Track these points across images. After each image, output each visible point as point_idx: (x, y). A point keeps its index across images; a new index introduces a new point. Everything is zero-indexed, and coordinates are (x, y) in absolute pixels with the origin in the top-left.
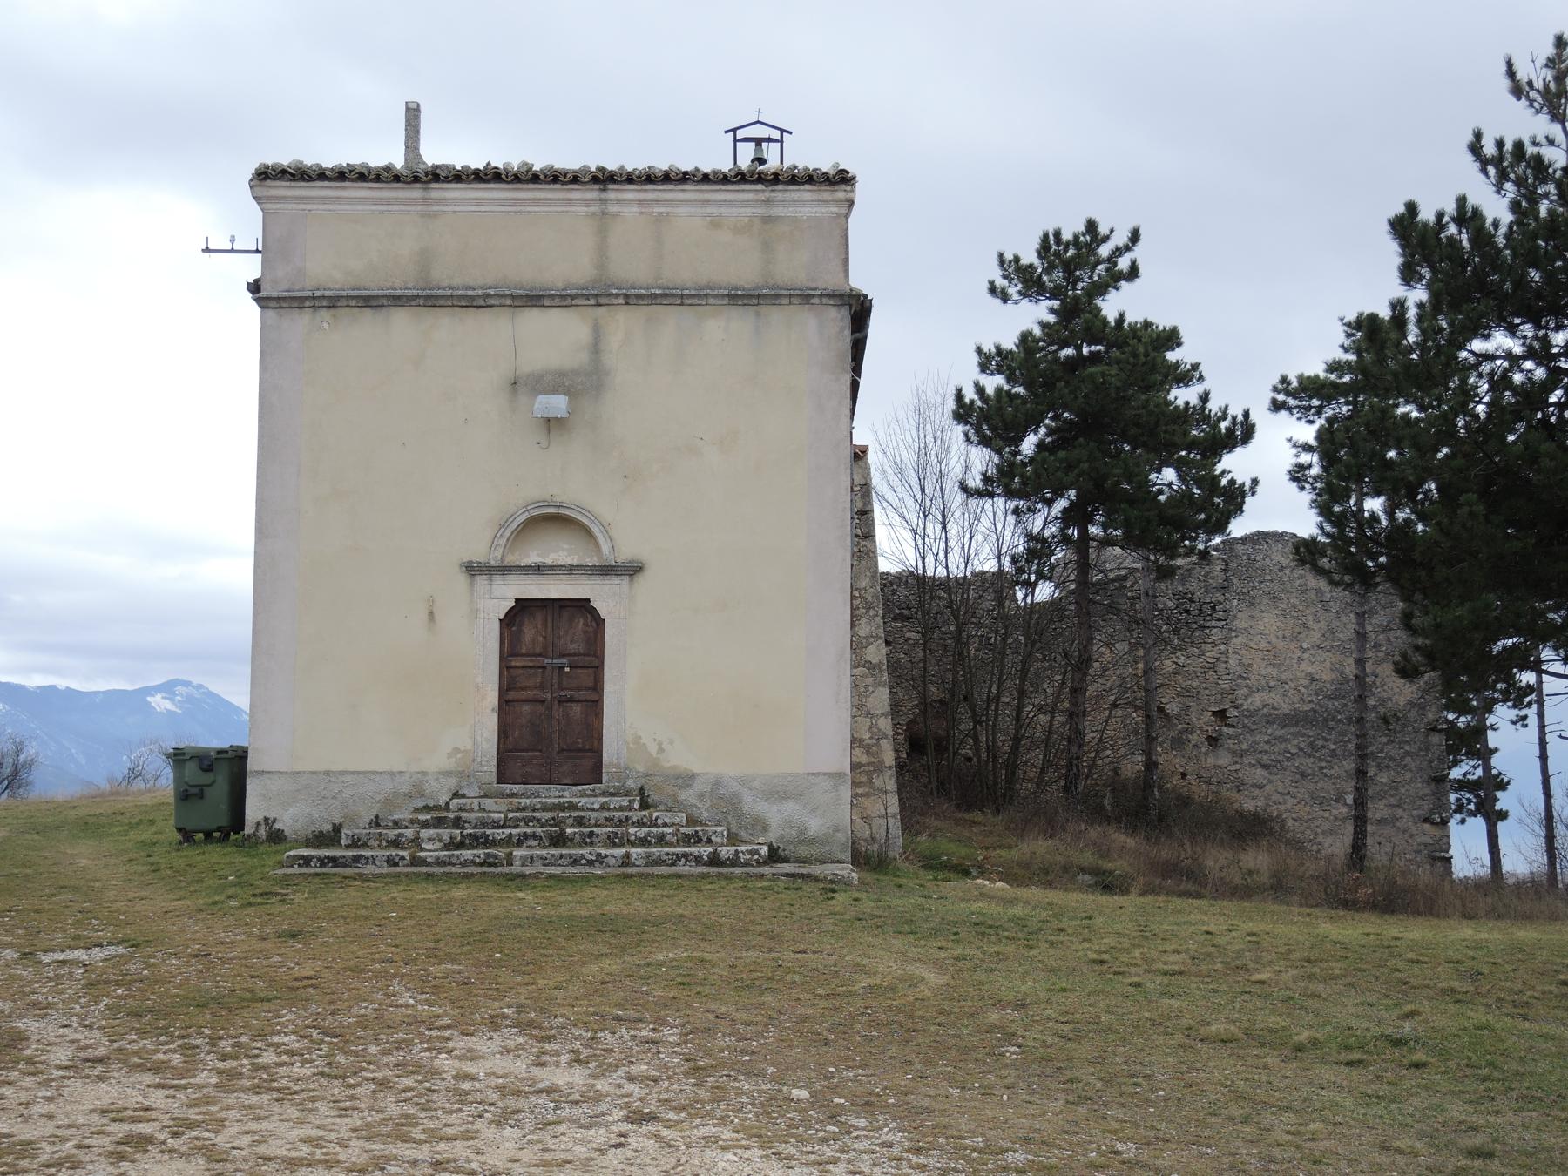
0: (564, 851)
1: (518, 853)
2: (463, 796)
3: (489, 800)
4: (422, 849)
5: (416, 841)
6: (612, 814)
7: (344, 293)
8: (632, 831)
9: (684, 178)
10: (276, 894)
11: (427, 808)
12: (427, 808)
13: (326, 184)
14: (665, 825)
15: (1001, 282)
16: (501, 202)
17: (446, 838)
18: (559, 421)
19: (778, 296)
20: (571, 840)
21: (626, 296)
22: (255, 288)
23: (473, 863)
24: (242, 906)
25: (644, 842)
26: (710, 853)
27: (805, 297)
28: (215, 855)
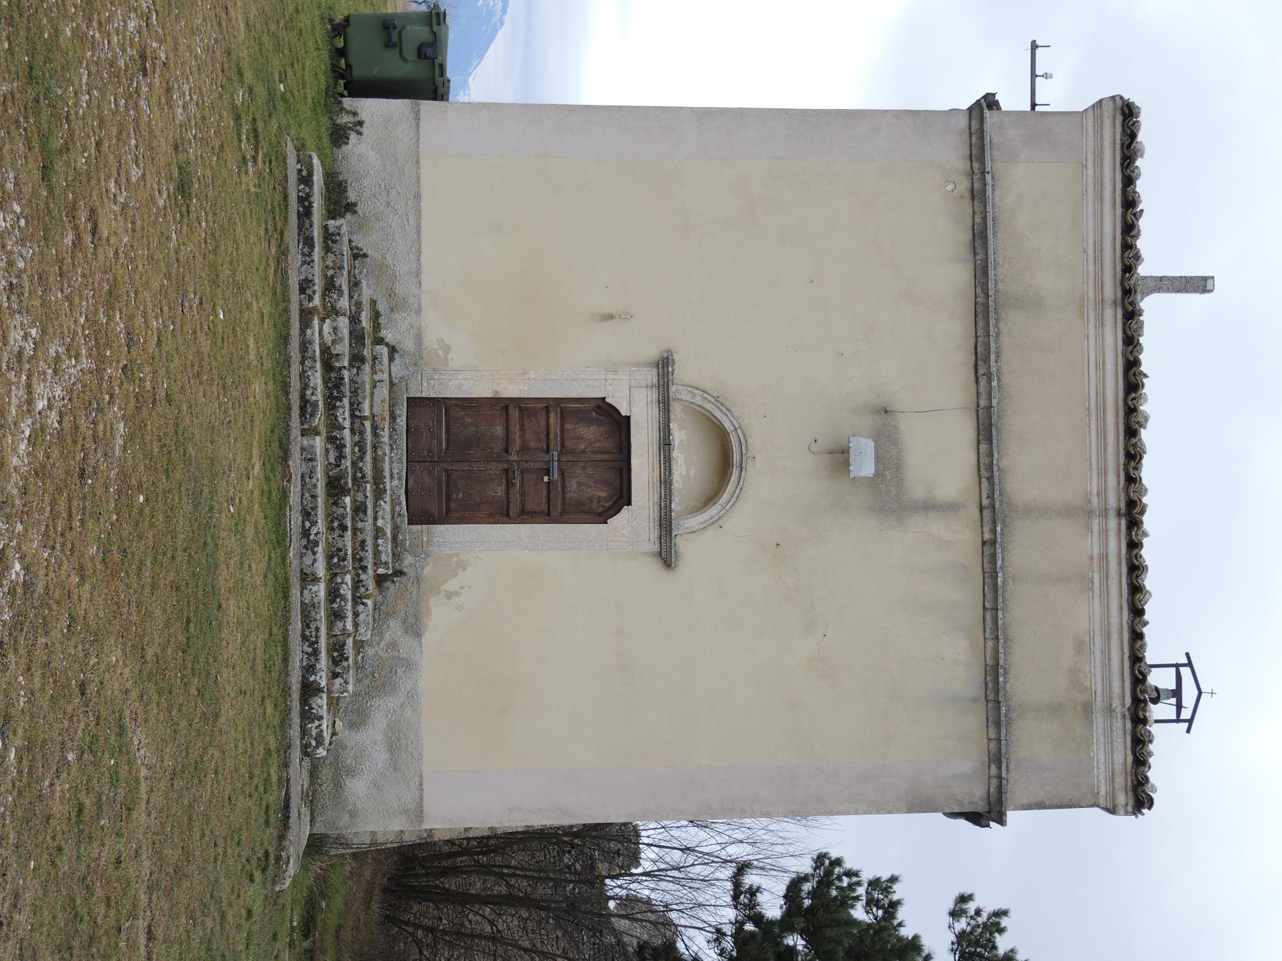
0: (320, 501)
1: (319, 443)
2: (391, 359)
3: (386, 392)
4: (322, 320)
5: (333, 312)
6: (370, 548)
7: (989, 209)
8: (348, 578)
9: (1137, 612)
10: (256, 149)
11: (376, 315)
12: (376, 315)
13: (1119, 186)
14: (356, 615)
15: (971, 907)
16: (1101, 392)
17: (337, 349)
18: (846, 464)
19: (998, 724)
20: (336, 504)
21: (993, 542)
22: (990, 102)
23: (305, 387)
24: (234, 108)
25: (333, 594)
26: (323, 658)
27: (997, 758)
28: (315, 63)
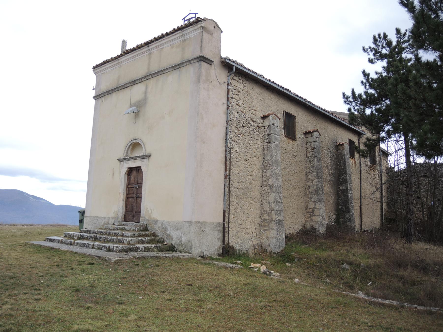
19: (183, 63)
